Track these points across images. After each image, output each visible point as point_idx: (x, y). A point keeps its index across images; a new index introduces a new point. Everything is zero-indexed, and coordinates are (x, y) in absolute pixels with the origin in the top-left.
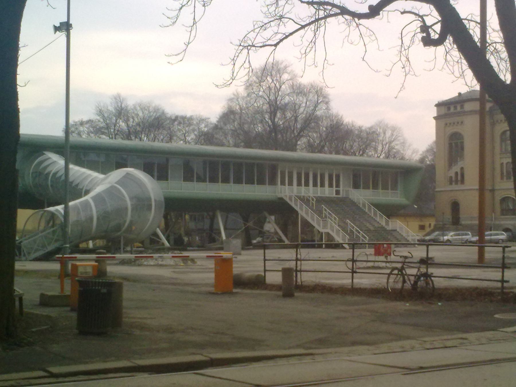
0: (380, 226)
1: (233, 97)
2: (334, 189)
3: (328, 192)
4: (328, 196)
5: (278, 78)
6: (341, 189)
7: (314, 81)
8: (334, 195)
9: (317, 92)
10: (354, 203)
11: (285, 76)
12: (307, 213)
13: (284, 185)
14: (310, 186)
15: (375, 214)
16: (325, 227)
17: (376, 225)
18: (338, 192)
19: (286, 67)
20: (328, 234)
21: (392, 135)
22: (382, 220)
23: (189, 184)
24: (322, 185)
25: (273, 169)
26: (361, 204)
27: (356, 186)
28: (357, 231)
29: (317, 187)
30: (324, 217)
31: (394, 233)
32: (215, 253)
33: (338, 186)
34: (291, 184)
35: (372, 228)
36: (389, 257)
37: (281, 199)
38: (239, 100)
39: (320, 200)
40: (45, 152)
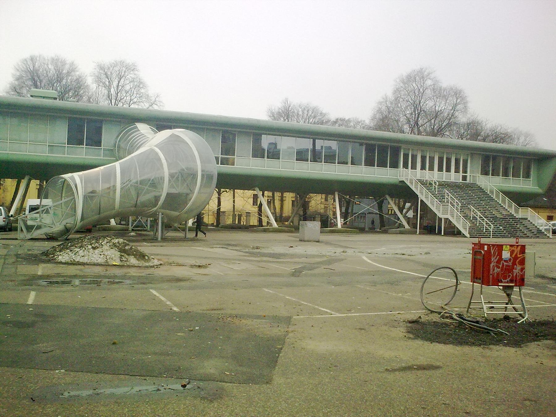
0: (509, 213)
1: (382, 100)
2: (461, 174)
3: (454, 177)
4: (454, 181)
5: (422, 84)
6: (468, 175)
7: (454, 85)
8: (461, 181)
9: (456, 94)
10: (480, 189)
11: (429, 82)
12: (427, 197)
13: (407, 168)
14: (435, 170)
15: (504, 201)
16: (445, 212)
17: (505, 213)
18: (464, 178)
19: (429, 74)
20: (446, 219)
21: (525, 140)
22: (511, 208)
23: (258, 160)
24: (448, 170)
25: (396, 151)
26: (489, 191)
27: (485, 172)
28: (480, 217)
29: (450, 172)
30: (446, 202)
31: (524, 222)
32: (140, 273)
33: (465, 171)
34: (414, 167)
35: (499, 216)
36: (516, 289)
37: (402, 182)
38: (387, 103)
39: (443, 185)
40: (136, 123)
